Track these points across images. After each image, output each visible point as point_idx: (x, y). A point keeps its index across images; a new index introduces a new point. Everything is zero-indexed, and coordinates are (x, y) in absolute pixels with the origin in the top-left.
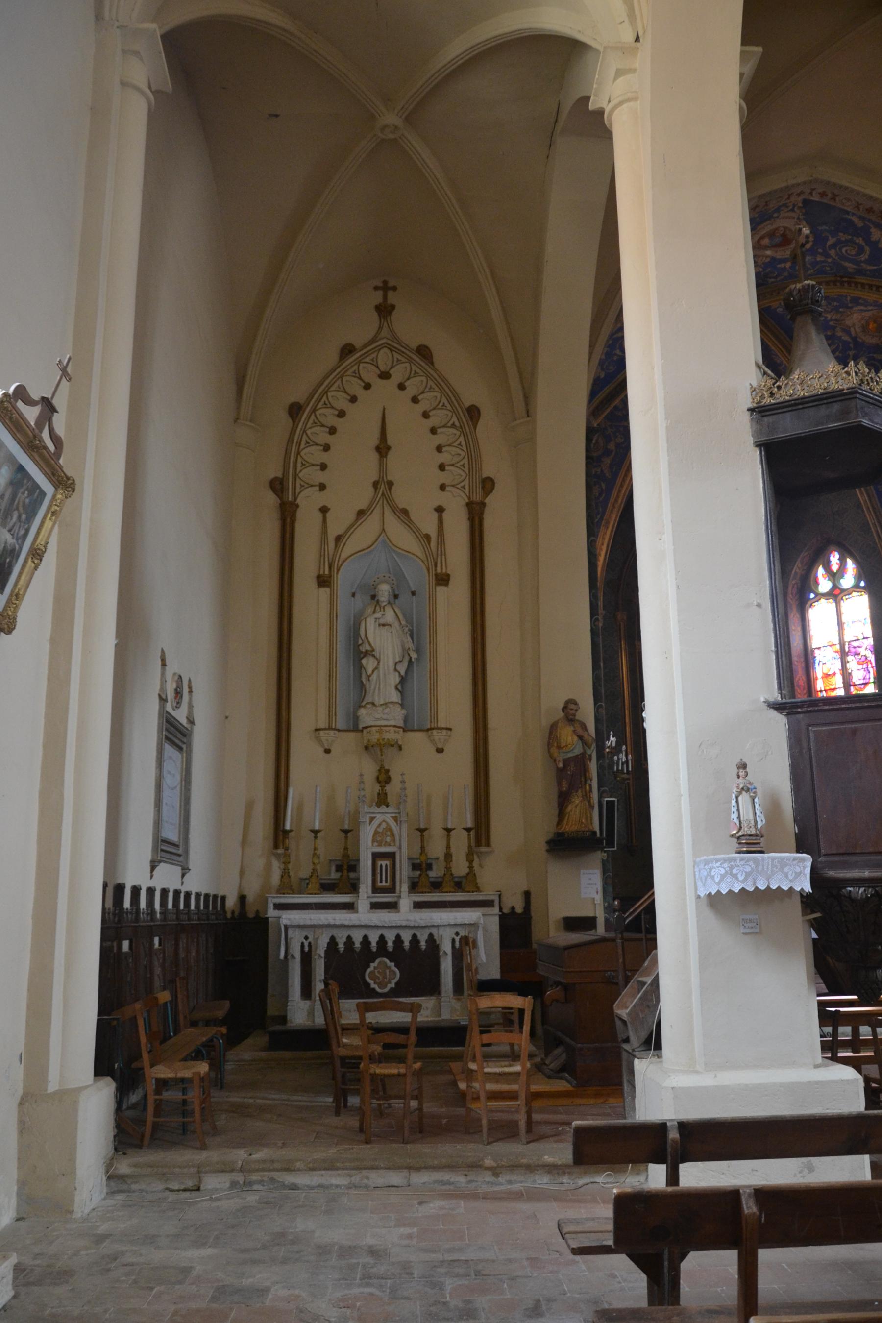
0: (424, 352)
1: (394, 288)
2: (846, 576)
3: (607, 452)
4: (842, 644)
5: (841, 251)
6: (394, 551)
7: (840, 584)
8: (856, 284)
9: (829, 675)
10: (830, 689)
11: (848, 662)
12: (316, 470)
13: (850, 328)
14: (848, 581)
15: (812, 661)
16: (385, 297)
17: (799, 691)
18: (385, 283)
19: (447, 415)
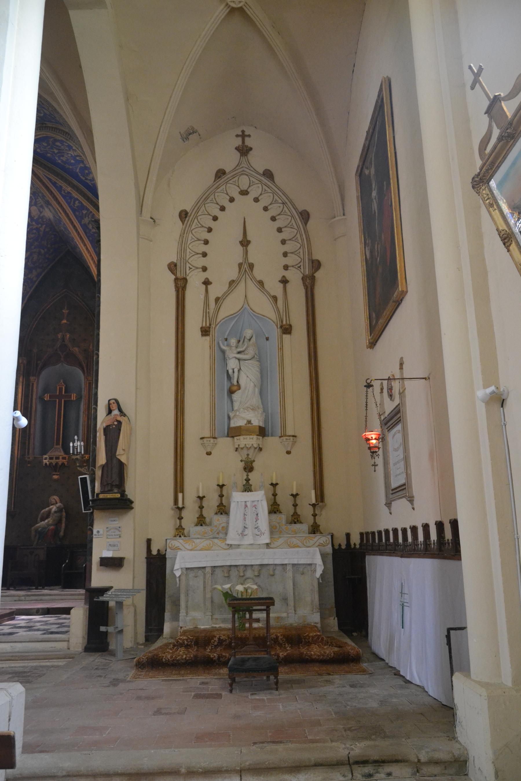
0: (268, 174)
1: (249, 136)
6: (255, 316)
12: (200, 257)
16: (243, 142)
18: (243, 132)
19: (259, 187)
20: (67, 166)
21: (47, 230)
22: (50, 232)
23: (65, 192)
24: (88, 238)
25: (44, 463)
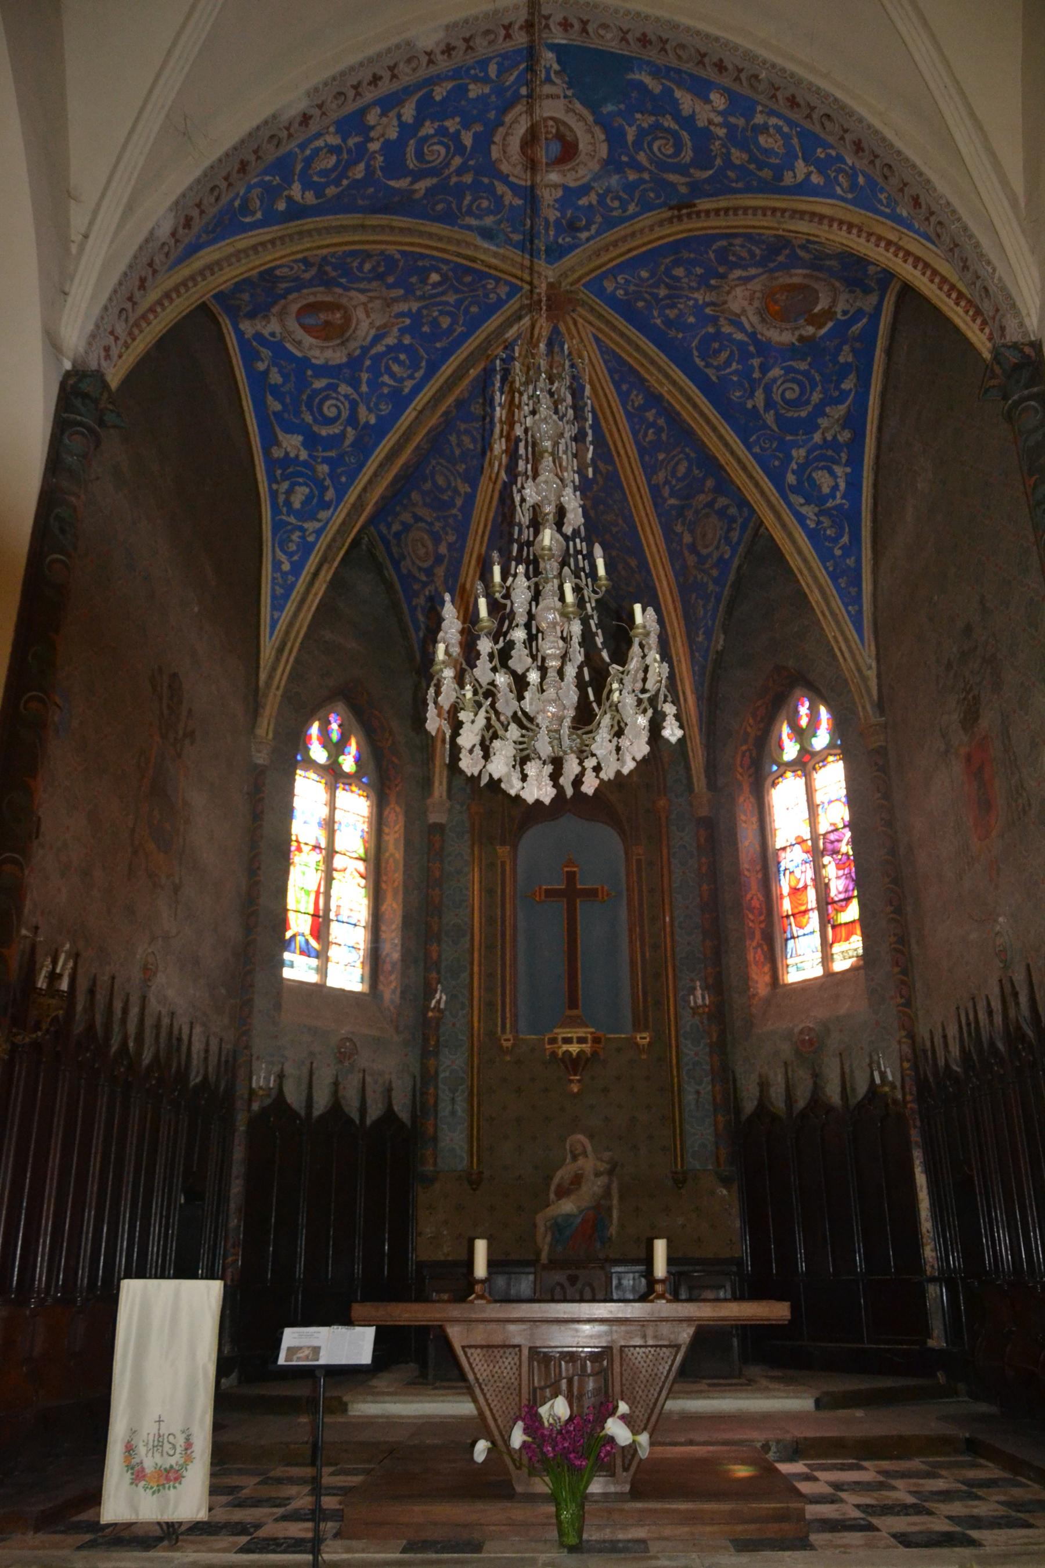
2: (819, 732)
3: (439, 559)
4: (815, 836)
5: (651, 149)
7: (811, 745)
8: (698, 214)
9: (798, 890)
10: (800, 912)
11: (824, 866)
13: (738, 316)
14: (821, 740)
15: (774, 869)
17: (751, 916)
20: (672, 333)
23: (633, 405)
24: (659, 516)
25: (548, 1053)
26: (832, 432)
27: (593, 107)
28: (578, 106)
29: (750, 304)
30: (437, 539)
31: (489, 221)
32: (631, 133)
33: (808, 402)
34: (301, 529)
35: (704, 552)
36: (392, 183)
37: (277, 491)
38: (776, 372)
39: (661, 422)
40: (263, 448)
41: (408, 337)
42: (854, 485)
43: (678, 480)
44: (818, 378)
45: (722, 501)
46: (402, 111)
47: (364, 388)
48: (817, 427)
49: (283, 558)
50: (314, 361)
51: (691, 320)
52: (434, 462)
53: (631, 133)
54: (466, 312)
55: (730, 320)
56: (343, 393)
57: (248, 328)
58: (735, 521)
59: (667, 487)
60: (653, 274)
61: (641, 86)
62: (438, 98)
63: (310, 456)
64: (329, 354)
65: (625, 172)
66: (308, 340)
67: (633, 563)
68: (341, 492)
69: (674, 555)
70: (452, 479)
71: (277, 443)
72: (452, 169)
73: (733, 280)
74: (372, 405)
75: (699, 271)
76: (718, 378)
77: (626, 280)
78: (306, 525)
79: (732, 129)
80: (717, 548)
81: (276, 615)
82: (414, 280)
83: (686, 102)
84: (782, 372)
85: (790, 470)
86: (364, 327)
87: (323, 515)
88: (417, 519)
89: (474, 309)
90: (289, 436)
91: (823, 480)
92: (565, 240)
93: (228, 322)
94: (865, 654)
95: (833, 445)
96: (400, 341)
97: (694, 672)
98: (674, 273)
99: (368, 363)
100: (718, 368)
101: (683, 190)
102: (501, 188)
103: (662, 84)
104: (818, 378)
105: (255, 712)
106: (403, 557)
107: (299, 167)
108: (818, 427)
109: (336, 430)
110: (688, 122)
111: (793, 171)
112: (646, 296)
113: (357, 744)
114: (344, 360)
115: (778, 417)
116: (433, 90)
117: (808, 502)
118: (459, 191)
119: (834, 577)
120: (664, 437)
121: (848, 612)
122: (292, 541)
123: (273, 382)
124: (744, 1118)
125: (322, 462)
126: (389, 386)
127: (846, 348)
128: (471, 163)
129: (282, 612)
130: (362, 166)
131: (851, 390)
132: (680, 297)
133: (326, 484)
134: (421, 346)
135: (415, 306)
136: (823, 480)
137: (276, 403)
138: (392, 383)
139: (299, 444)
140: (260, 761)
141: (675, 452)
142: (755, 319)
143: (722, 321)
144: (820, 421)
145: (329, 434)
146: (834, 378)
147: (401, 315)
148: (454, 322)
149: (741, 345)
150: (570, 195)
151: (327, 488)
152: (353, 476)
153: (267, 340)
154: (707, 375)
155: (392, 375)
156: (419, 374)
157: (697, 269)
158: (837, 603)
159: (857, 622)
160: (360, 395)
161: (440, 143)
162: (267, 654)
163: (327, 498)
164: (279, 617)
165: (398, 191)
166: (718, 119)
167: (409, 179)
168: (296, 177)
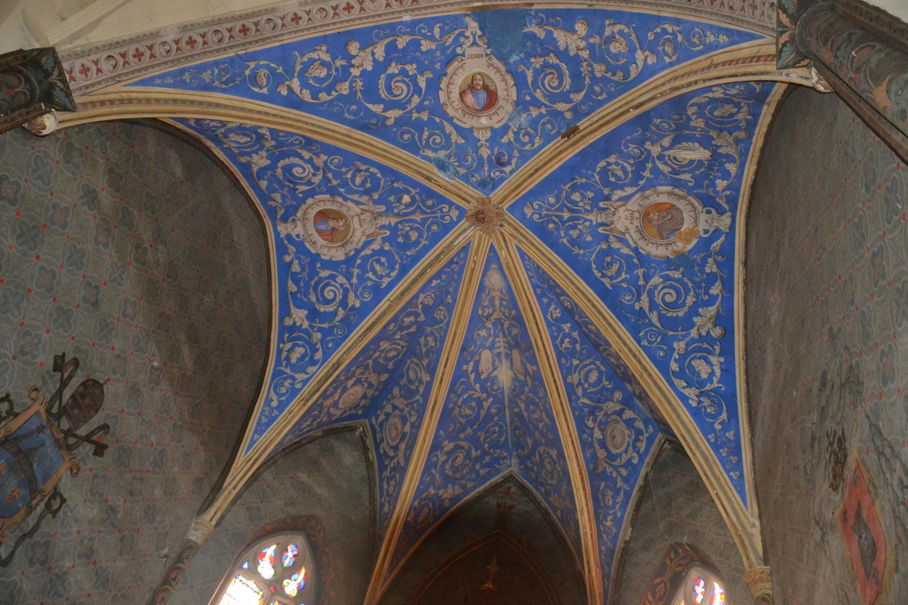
3: (404, 435)
20: (576, 250)
21: (493, 411)
22: (496, 418)
23: (552, 316)
24: (573, 409)
26: (706, 329)
27: (503, 59)
28: (495, 61)
29: (631, 223)
30: (404, 420)
31: (442, 154)
32: (530, 74)
33: (684, 304)
34: (293, 378)
35: (614, 451)
36: (370, 106)
37: (282, 348)
38: (656, 280)
39: (575, 334)
40: (280, 316)
41: (388, 244)
42: (728, 371)
43: (590, 385)
44: (690, 285)
45: (628, 414)
46: (375, 51)
47: (355, 280)
48: (693, 325)
49: (275, 397)
50: (322, 257)
51: (589, 238)
52: (409, 361)
53: (530, 74)
54: (429, 229)
55: (617, 237)
56: (340, 282)
57: (283, 229)
58: (642, 435)
59: (580, 388)
60: (558, 198)
61: (532, 36)
62: (400, 47)
63: (310, 326)
64: (333, 252)
65: (529, 111)
66: (321, 241)
67: (554, 453)
68: (327, 355)
69: (586, 445)
70: (419, 372)
71: (290, 316)
72: (413, 105)
73: (616, 201)
74: (358, 293)
75: (590, 194)
76: (612, 285)
77: (539, 205)
78: (297, 376)
79: (591, 47)
80: (626, 451)
81: (256, 436)
82: (392, 199)
83: (562, 38)
84: (661, 280)
85: (673, 359)
86: (358, 237)
87: (311, 370)
88: (395, 408)
89: (434, 228)
90: (298, 310)
91: (700, 367)
92: (496, 174)
93: (269, 221)
94: (748, 515)
95: (708, 338)
96: (382, 247)
97: (600, 551)
98: (572, 198)
99: (359, 261)
100: (611, 278)
101: (568, 115)
102: (449, 128)
103: (546, 30)
104: (690, 285)
105: (208, 503)
106: (382, 440)
107: (298, 68)
108: (693, 325)
109: (330, 308)
110: (563, 55)
111: (635, 63)
112: (554, 218)
113: (306, 575)
114: (343, 258)
115: (661, 317)
116: (396, 40)
117: (689, 385)
118: (419, 126)
119: (716, 447)
120: (578, 347)
121: (731, 478)
122: (284, 386)
123: (294, 270)
124: (63, 404)
125: (317, 332)
126: (372, 280)
127: (710, 260)
128: (426, 103)
129: (261, 436)
130: (346, 85)
131: (718, 295)
132: (578, 219)
133: (317, 347)
134: (398, 254)
135: (394, 221)
136: (700, 367)
137: (294, 285)
138: (374, 278)
139: (304, 316)
140: (193, 538)
141: (587, 362)
142: (636, 236)
143: (612, 239)
144: (695, 319)
145: (325, 311)
146: (703, 285)
147: (383, 227)
148: (420, 236)
149: (628, 258)
150: (497, 134)
151: (317, 350)
152: (337, 345)
153: (294, 239)
154: (603, 283)
155: (375, 273)
156: (393, 274)
157: (589, 193)
158: (719, 469)
159: (739, 485)
160: (351, 285)
161: (403, 82)
162: (238, 466)
163: (316, 358)
164: (258, 439)
165: (374, 115)
166: (583, 44)
167: (382, 106)
168: (296, 74)
